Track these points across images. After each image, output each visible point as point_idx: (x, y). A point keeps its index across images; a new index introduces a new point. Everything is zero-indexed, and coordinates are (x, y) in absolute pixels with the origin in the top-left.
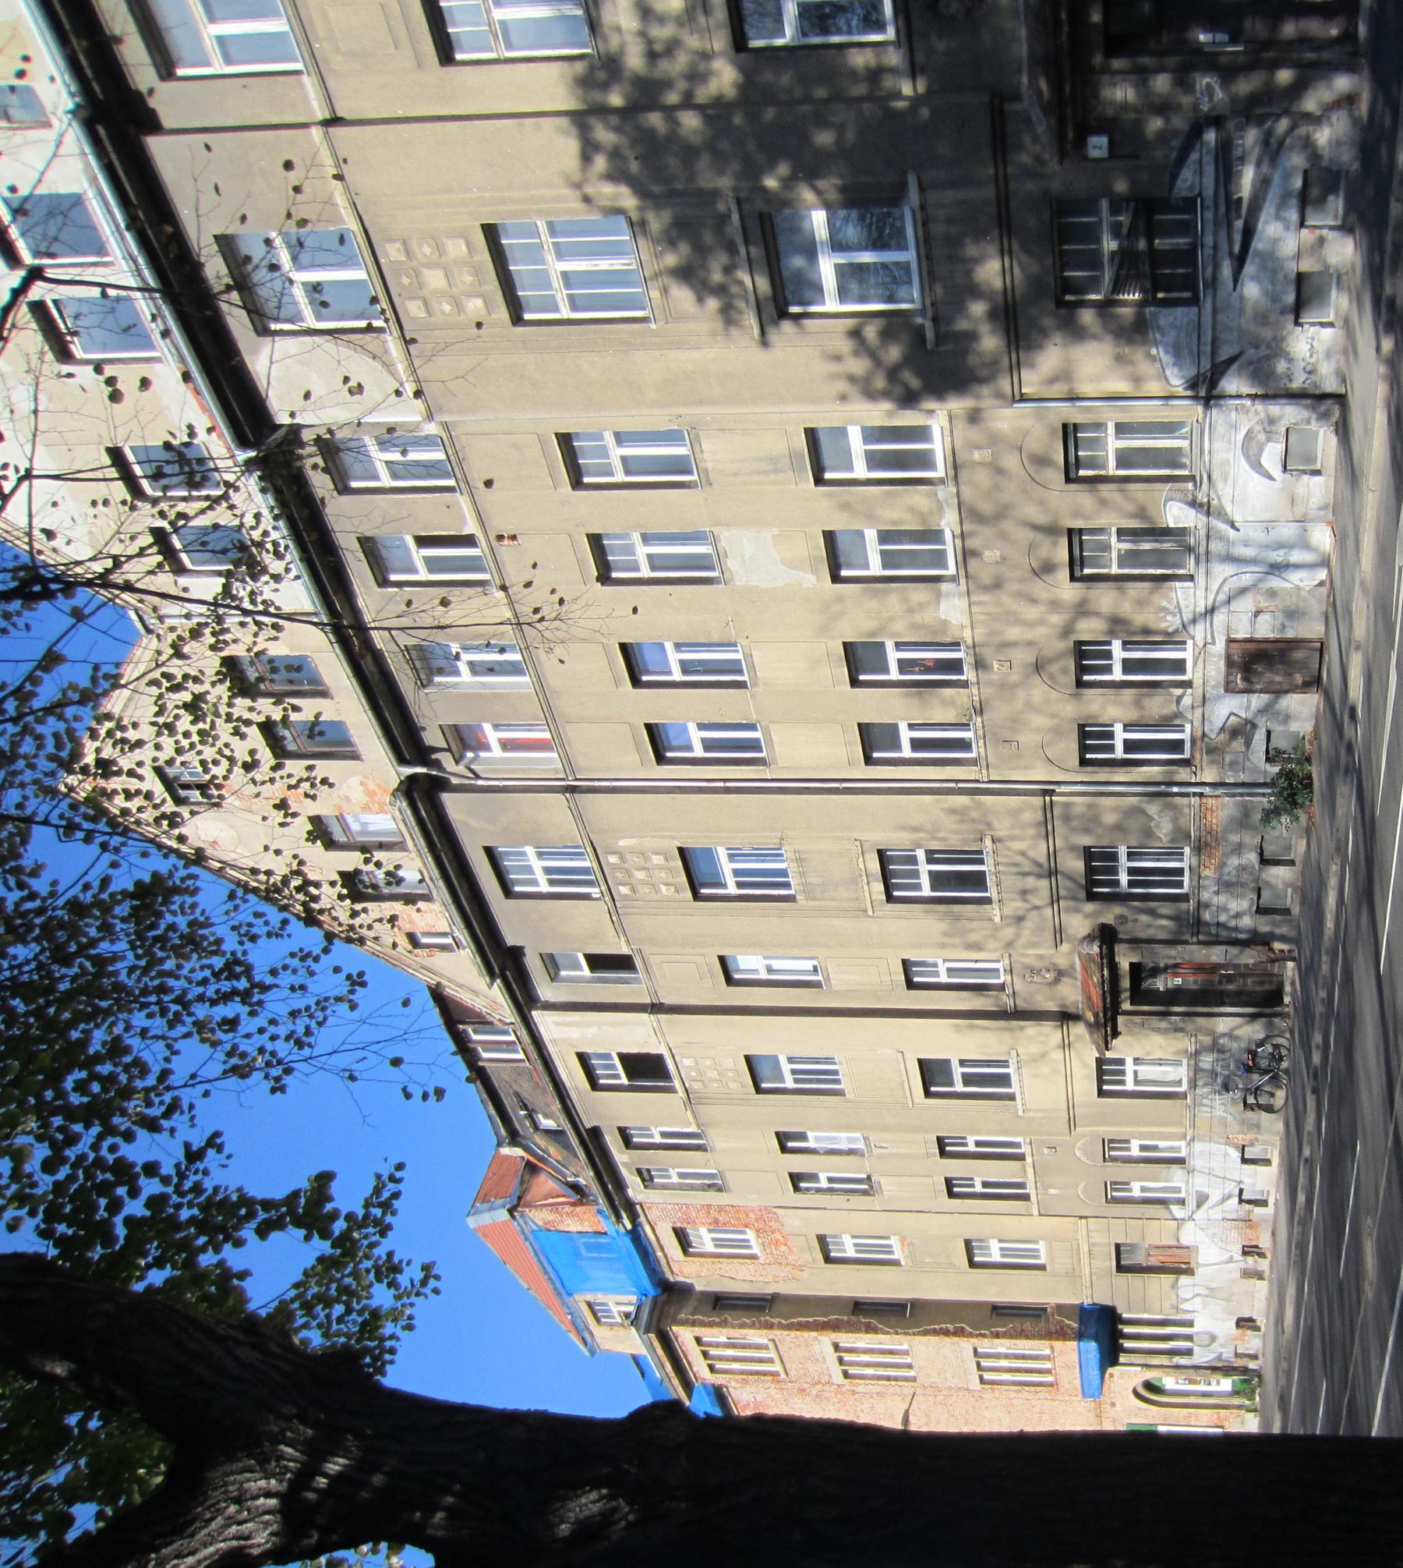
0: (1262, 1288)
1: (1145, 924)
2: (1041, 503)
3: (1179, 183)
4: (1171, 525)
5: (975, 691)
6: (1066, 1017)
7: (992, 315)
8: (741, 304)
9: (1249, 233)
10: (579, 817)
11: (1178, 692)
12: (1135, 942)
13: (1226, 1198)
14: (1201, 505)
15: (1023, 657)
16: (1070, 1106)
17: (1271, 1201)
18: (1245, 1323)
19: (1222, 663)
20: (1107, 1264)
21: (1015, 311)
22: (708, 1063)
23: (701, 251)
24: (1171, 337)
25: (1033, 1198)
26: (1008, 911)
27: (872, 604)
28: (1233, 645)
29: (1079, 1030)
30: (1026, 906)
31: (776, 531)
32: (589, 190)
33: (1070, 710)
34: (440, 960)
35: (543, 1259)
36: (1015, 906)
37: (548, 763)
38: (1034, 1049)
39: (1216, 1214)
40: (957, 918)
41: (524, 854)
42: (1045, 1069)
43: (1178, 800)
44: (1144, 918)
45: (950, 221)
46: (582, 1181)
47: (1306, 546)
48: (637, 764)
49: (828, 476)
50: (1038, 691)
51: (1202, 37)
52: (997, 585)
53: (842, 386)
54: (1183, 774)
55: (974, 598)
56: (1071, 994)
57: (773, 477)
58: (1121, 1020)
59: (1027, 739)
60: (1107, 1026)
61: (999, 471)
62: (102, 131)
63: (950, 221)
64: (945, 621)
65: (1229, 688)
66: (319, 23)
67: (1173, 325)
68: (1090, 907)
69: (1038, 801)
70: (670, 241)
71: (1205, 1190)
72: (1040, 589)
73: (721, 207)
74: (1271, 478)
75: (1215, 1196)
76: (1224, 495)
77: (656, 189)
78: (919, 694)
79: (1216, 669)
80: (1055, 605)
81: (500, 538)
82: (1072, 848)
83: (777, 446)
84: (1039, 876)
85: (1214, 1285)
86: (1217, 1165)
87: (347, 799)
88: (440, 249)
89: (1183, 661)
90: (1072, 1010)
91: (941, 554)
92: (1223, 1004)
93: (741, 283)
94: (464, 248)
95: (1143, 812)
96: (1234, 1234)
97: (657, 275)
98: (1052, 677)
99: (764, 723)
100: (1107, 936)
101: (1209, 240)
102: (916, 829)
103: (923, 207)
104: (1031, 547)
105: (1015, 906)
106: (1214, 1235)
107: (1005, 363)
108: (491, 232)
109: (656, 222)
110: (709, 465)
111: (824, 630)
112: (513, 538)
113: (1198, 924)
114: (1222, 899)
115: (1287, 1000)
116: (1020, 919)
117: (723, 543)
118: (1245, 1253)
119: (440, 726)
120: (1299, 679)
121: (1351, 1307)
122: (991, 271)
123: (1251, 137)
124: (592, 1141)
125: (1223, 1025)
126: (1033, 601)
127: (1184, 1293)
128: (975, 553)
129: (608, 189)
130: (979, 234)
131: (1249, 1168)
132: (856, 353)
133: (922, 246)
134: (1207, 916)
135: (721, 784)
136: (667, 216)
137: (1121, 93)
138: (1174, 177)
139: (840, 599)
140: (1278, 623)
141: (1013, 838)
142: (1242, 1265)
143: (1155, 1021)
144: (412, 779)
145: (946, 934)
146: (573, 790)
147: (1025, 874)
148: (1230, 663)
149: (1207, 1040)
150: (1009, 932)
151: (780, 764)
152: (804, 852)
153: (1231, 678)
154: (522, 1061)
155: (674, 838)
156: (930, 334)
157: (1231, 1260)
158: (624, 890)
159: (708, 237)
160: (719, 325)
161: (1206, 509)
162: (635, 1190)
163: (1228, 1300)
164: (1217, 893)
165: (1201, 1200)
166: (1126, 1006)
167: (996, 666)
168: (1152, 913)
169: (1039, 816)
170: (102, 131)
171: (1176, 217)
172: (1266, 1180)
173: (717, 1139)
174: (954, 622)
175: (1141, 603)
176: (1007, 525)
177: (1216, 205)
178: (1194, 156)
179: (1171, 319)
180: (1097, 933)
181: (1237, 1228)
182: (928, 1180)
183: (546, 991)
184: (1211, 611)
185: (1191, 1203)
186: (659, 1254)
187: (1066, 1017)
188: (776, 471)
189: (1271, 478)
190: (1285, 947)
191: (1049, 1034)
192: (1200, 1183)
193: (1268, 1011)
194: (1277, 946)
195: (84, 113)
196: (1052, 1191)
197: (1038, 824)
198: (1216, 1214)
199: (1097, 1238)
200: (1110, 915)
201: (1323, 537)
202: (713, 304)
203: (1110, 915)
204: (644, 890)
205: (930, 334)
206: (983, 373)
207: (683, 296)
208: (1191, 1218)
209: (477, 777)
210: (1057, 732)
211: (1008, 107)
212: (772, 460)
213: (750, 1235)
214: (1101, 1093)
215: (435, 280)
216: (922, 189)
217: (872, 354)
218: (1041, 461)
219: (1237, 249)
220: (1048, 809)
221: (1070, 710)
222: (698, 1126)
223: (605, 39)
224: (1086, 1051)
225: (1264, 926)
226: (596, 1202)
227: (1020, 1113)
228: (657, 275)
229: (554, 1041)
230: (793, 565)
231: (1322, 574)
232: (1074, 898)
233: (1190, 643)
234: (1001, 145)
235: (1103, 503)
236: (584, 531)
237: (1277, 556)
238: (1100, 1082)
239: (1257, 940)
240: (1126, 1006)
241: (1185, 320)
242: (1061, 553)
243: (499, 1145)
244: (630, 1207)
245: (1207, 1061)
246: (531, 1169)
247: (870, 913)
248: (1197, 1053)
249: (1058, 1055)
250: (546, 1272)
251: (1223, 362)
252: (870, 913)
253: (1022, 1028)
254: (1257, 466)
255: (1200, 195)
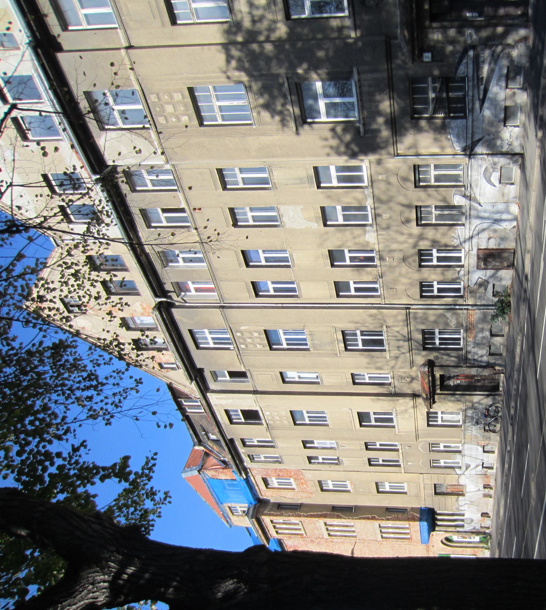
0: (491, 501)
1: (446, 360)
2: (405, 196)
3: (459, 71)
4: (456, 204)
5: (379, 269)
6: (415, 396)
7: (386, 123)
8: (289, 118)
9: (486, 91)
10: (225, 318)
11: (458, 269)
12: (442, 366)
13: (477, 466)
14: (467, 197)
15: (398, 256)
16: (416, 430)
17: (495, 467)
18: (485, 515)
19: (476, 258)
20: (431, 492)
21: (395, 121)
22: (276, 413)
23: (273, 98)
24: (456, 131)
25: (402, 466)
26: (392, 354)
27: (340, 235)
28: (480, 251)
29: (420, 401)
30: (399, 352)
31: (302, 207)
32: (229, 74)
33: (416, 276)
34: (171, 374)
35: (211, 490)
36: (395, 352)
37: (213, 297)
38: (403, 408)
39: (473, 472)
40: (372, 357)
41: (204, 332)
42: (407, 416)
43: (459, 311)
44: (445, 357)
45: (370, 86)
46: (226, 459)
47: (508, 212)
48: (248, 297)
49: (322, 185)
50: (404, 269)
51: (468, 15)
52: (388, 228)
53: (328, 150)
54: (460, 301)
55: (379, 233)
56: (417, 387)
57: (301, 185)
58: (436, 397)
59: (400, 287)
60: (431, 399)
61: (389, 183)
62: (40, 51)
63: (370, 86)
64: (368, 242)
65: (478, 268)
66: (124, 9)
67: (456, 127)
68: (424, 353)
69: (404, 312)
70: (261, 94)
71: (469, 463)
72: (405, 229)
73: (281, 81)
74: (495, 186)
75: (473, 465)
76: (476, 192)
77: (255, 73)
78: (358, 270)
79: (473, 260)
80: (410, 235)
81: (195, 209)
82: (417, 330)
83: (302, 173)
84: (404, 341)
85: (472, 500)
86: (474, 453)
87: (135, 311)
88: (171, 97)
89: (461, 257)
90: (417, 393)
91: (366, 216)
92: (476, 391)
93: (288, 110)
94: (181, 96)
95: (445, 316)
96: (480, 480)
97: (256, 107)
98: (409, 263)
99: (297, 281)
100: (431, 364)
101: (470, 93)
102: (356, 323)
103: (359, 81)
104: (401, 213)
105: (395, 352)
106: (473, 480)
107: (391, 141)
108: (191, 90)
109: (255, 86)
110: (276, 181)
111: (321, 245)
112: (200, 209)
113: (466, 360)
114: (475, 350)
115: (501, 389)
116: (397, 358)
117: (281, 211)
118: (484, 487)
119: (171, 283)
120: (505, 264)
121: (526, 509)
122: (386, 105)
123: (487, 53)
124: (230, 444)
125: (476, 399)
126: (402, 234)
127: (461, 503)
128: (379, 215)
129: (237, 74)
130: (381, 91)
131: (486, 454)
132: (333, 137)
133: (359, 96)
134: (470, 356)
135: (281, 305)
136: (259, 84)
137: (436, 36)
138: (457, 69)
139: (327, 233)
140: (497, 242)
141: (394, 326)
142: (483, 492)
143: (449, 397)
144: (160, 303)
145: (368, 363)
146: (223, 307)
147: (399, 340)
148: (479, 258)
149: (470, 404)
150: (392, 363)
151: (304, 297)
152: (313, 331)
153: (479, 264)
154: (203, 413)
155: (262, 326)
156: (362, 130)
157: (479, 490)
158: (243, 346)
159: (276, 92)
160: (280, 126)
161: (469, 198)
162: (247, 463)
163: (478, 506)
164: (474, 347)
165: (468, 467)
166: (438, 391)
167: (387, 259)
168: (448, 355)
169: (405, 317)
170: (40, 51)
171: (458, 84)
172: (493, 459)
173: (279, 443)
174: (371, 242)
175: (444, 235)
176: (392, 204)
177: (473, 80)
178: (465, 61)
179: (456, 124)
180: (427, 363)
181: (481, 478)
182: (361, 459)
183: (212, 386)
184: (471, 238)
185: (464, 468)
186: (257, 488)
187: (415, 396)
188: (302, 183)
189: (495, 186)
190: (500, 368)
191: (408, 402)
192: (467, 460)
193: (493, 393)
194: (497, 368)
195: (33, 44)
196: (409, 463)
197: (404, 321)
198: (473, 472)
199: (427, 482)
200: (432, 356)
201: (515, 209)
202: (277, 118)
203: (432, 356)
204: (251, 346)
205: (362, 130)
206: (383, 145)
207: (266, 115)
208: (463, 474)
209: (186, 302)
210: (411, 285)
211: (392, 42)
212: (300, 179)
213: (292, 480)
214: (429, 425)
215: (169, 109)
216: (359, 73)
217: (339, 138)
218: (405, 179)
219: (481, 97)
220: (408, 315)
221: (416, 276)
222: (272, 438)
223: (235, 15)
224: (423, 409)
225: (492, 360)
226: (232, 468)
227: (397, 433)
228: (256, 107)
229: (216, 405)
230: (309, 220)
231: (515, 223)
232: (418, 349)
233: (463, 250)
234: (389, 56)
235: (429, 196)
236: (227, 207)
237: (497, 216)
238: (428, 421)
239: (489, 366)
240: (438, 391)
241: (461, 125)
242: (413, 215)
243: (194, 445)
244: (245, 470)
245: (470, 413)
246: (207, 455)
247: (339, 355)
248: (466, 410)
249: (412, 410)
250: (212, 495)
251: (476, 141)
252: (339, 355)
253: (398, 400)
254: (489, 181)
255: (467, 76)
